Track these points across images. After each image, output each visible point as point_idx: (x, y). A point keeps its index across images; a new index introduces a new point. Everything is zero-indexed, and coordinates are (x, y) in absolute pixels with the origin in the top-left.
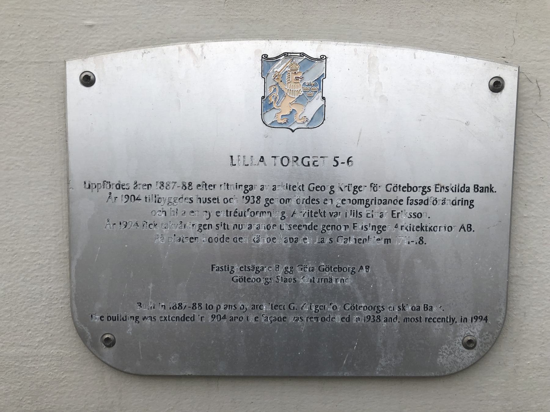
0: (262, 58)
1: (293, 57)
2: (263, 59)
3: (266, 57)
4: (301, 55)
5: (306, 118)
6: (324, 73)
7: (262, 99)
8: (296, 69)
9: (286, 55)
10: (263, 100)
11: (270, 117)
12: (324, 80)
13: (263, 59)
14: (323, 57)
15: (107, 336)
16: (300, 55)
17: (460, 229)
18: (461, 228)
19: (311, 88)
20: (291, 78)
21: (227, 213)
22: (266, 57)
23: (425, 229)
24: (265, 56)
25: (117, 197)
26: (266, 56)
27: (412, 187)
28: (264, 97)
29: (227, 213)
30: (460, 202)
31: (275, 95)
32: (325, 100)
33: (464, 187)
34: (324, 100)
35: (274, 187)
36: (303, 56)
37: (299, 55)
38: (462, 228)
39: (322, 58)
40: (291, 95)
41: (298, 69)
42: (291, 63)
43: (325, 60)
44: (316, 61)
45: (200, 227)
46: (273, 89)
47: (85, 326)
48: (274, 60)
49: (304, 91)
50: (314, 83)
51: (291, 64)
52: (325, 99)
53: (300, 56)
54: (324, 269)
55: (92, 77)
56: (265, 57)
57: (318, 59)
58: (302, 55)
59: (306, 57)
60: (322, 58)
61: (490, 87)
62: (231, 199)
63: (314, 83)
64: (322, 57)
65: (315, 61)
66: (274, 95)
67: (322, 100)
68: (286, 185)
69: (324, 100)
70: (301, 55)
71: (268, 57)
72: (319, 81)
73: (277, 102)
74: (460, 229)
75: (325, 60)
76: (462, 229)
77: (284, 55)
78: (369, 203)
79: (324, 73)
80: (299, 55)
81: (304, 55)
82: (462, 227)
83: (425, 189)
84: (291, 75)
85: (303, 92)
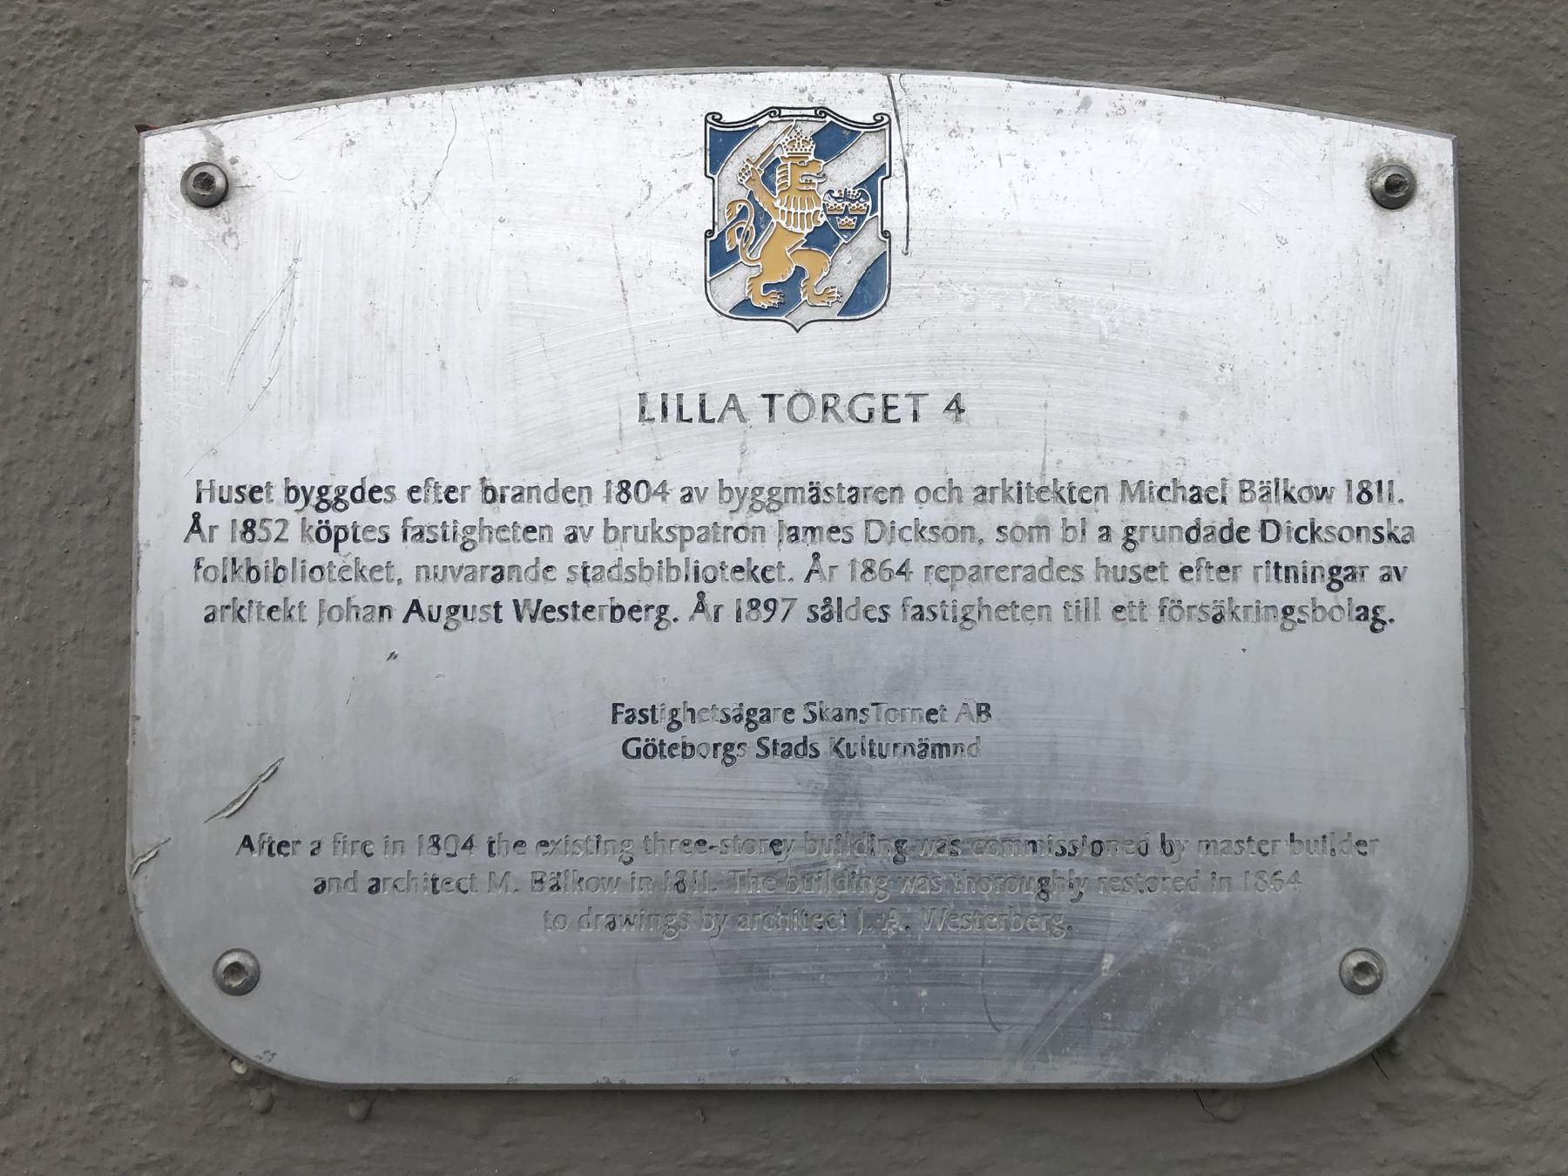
0: (706, 121)
1: (795, 119)
2: (709, 126)
3: (718, 121)
4: (818, 113)
5: (836, 290)
6: (885, 164)
7: (706, 237)
8: (803, 151)
9: (775, 112)
10: (709, 240)
11: (734, 284)
12: (711, 181)
13: (709, 126)
14: (883, 119)
15: (229, 960)
16: (816, 112)
17: (408, 616)
18: (411, 611)
19: (850, 205)
20: (789, 178)
21: (1277, 573)
22: (718, 121)
23: (1241, 615)
24: (713, 118)
25: (216, 527)
26: (717, 117)
27: (932, 489)
28: (711, 232)
29: (1277, 573)
30: (631, 533)
31: (744, 226)
32: (889, 237)
33: (555, 487)
34: (887, 240)
35: (854, 491)
36: (823, 115)
37: (782, 110)
38: (415, 612)
39: (878, 121)
40: (791, 226)
41: (810, 154)
42: (791, 137)
43: (886, 127)
44: (863, 131)
45: (454, 614)
46: (738, 210)
47: (745, 931)
48: (736, 129)
49: (828, 215)
50: (856, 191)
51: (790, 140)
52: (890, 234)
53: (816, 116)
54: (638, 750)
55: (219, 182)
56: (714, 118)
57: (869, 125)
58: (821, 113)
59: (834, 121)
60: (878, 121)
61: (1378, 197)
62: (1302, 530)
63: (856, 191)
64: (878, 118)
65: (860, 130)
66: (741, 226)
67: (882, 238)
68: (1016, 487)
69: (887, 240)
70: (818, 113)
71: (722, 121)
72: (871, 186)
73: (752, 246)
74: (408, 616)
75: (886, 127)
76: (412, 615)
77: (769, 114)
78: (1136, 537)
79: (885, 164)
80: (812, 112)
81: (826, 114)
82: (415, 608)
83: (326, 494)
84: (789, 169)
85: (825, 218)
